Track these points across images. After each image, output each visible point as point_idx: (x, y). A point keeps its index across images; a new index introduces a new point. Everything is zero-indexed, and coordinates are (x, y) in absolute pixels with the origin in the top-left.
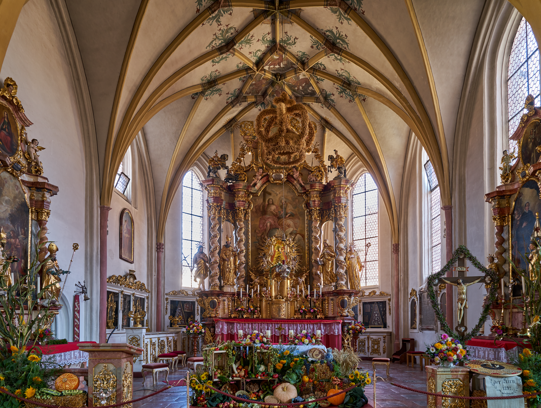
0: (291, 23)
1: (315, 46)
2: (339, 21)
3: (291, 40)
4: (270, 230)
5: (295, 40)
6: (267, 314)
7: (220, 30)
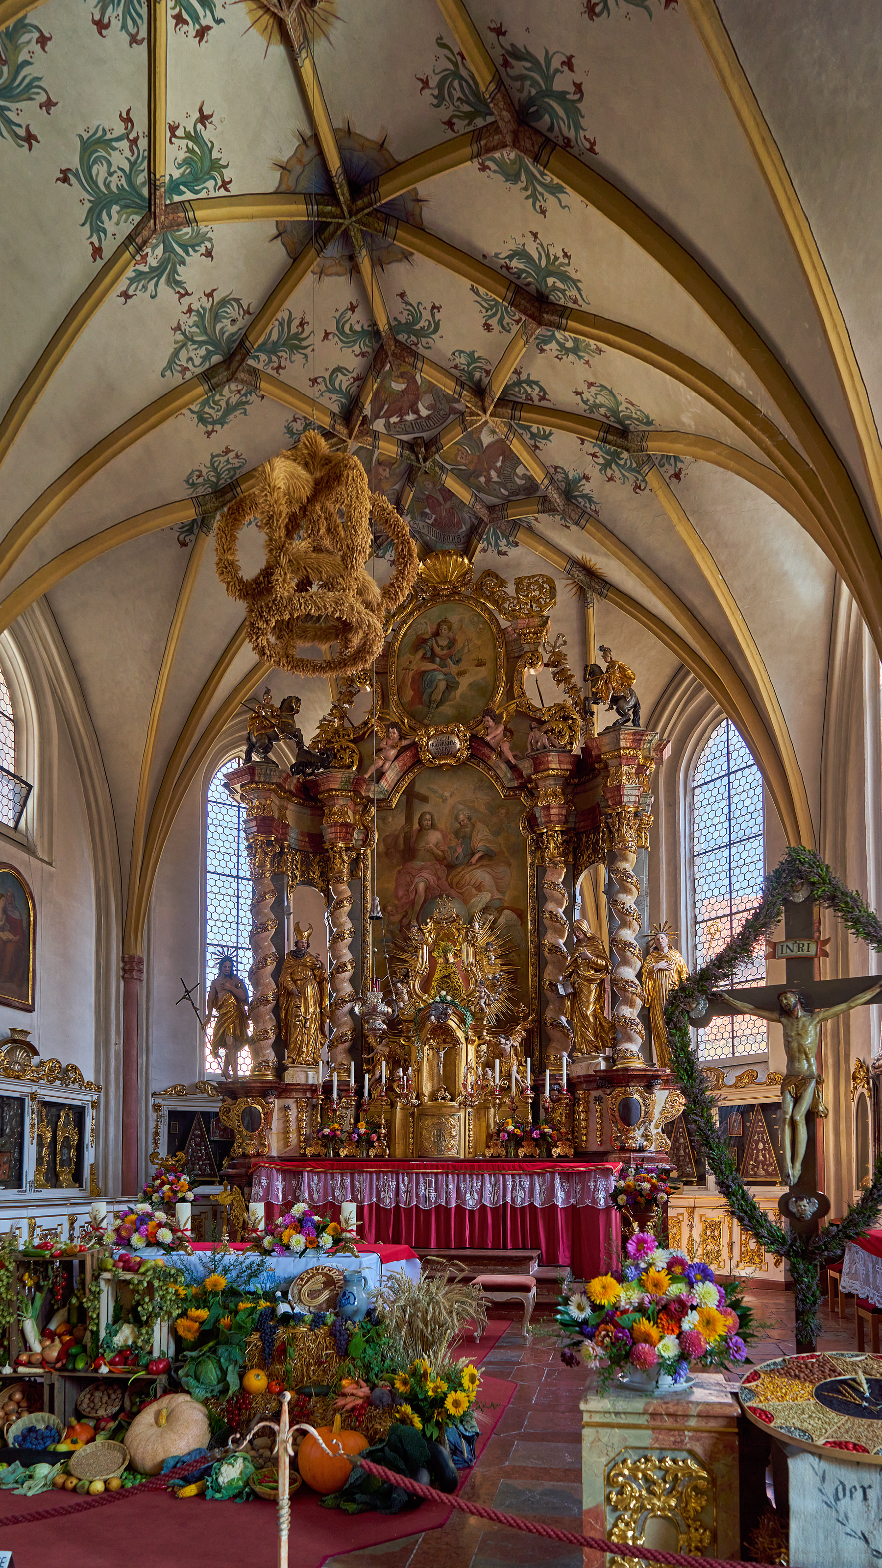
0: (406, 256)
1: (494, 322)
2: (534, 205)
3: (425, 316)
4: (425, 901)
5: (433, 315)
6: (406, 1144)
7: (190, 310)
